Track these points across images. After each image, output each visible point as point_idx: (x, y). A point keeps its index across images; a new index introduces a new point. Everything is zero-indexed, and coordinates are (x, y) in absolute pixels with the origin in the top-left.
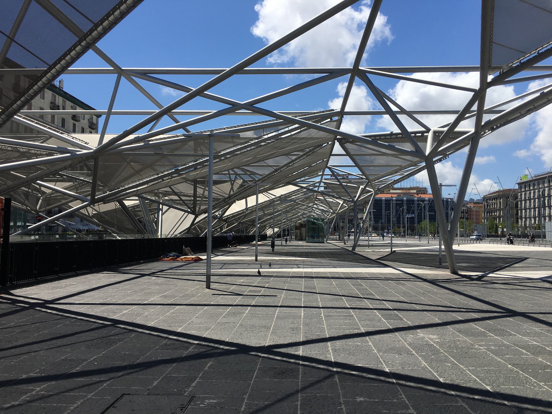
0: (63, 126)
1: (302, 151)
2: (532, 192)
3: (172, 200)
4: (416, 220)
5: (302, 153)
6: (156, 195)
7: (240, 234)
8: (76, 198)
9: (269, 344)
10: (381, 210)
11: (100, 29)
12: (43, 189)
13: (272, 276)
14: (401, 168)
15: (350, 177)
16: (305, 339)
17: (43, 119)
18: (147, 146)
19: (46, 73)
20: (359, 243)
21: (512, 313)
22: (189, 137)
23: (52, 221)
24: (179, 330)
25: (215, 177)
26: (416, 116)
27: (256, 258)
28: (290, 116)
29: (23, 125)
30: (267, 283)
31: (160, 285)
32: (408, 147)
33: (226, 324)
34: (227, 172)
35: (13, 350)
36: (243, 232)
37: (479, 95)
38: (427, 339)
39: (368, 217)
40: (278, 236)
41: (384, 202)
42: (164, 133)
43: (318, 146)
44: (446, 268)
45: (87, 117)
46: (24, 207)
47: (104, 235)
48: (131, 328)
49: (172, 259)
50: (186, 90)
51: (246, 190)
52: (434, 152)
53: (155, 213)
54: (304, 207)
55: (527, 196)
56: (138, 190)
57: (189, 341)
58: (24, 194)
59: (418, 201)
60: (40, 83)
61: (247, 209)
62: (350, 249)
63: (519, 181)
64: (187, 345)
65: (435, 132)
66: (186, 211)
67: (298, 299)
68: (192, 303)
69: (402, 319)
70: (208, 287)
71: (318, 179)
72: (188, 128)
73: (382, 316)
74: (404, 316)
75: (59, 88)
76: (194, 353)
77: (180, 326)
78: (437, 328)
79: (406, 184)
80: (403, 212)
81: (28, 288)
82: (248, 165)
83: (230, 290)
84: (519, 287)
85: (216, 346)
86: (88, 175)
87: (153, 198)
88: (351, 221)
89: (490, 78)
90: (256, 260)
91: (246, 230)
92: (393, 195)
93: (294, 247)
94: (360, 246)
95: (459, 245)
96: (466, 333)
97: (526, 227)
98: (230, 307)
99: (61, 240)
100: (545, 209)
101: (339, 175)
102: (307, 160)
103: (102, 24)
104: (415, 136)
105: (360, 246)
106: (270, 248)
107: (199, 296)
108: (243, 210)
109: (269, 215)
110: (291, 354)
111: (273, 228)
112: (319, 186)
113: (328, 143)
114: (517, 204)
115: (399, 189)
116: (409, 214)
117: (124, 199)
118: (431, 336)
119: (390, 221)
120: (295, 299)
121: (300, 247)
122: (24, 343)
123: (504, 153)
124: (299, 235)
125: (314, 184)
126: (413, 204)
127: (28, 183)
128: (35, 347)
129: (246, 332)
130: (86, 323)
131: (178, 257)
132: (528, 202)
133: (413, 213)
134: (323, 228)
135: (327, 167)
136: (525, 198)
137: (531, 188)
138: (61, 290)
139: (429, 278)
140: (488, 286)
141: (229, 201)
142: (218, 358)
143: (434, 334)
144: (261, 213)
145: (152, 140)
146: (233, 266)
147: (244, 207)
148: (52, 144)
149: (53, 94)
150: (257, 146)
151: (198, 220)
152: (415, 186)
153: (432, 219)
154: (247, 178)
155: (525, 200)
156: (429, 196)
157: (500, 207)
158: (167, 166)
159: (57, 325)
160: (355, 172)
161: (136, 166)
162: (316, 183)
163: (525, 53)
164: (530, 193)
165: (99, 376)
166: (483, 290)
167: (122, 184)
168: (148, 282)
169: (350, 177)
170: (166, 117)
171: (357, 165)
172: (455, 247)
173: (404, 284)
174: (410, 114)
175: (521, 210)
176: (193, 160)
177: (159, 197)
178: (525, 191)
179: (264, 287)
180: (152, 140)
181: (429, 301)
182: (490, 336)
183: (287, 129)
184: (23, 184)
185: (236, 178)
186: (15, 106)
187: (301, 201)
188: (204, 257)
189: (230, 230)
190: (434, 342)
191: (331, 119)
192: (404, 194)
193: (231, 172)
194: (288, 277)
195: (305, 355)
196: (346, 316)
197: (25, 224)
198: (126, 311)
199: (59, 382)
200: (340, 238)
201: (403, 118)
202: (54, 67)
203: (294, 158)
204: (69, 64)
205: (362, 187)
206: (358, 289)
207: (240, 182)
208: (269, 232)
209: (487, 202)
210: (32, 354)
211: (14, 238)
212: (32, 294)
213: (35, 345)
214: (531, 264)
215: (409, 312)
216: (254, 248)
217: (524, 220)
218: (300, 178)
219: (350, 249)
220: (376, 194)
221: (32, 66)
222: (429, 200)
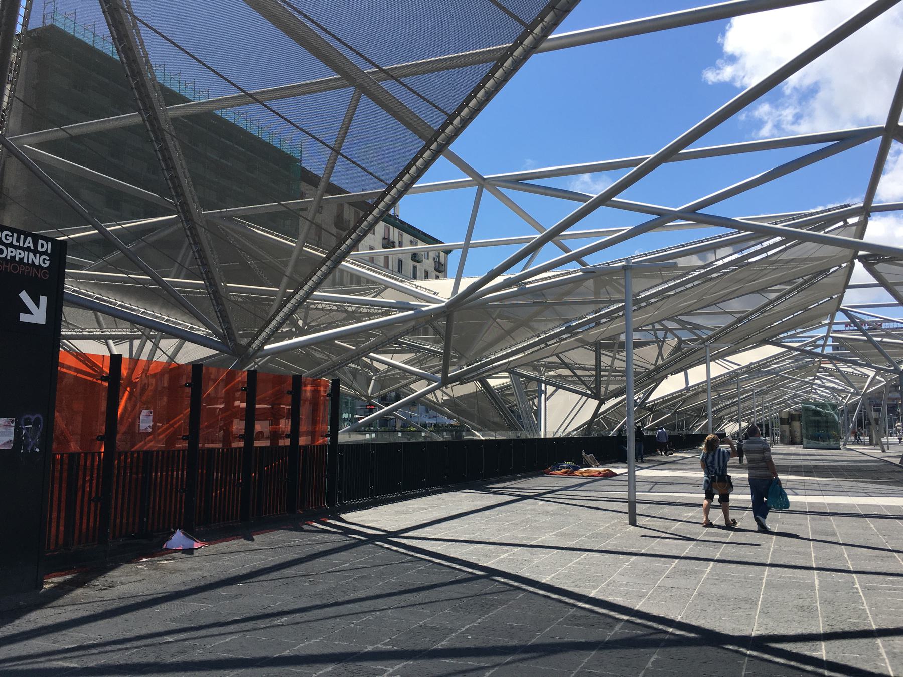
0: (400, 270)
1: (788, 282)
3: (560, 376)
5: (788, 288)
6: (536, 368)
7: (676, 432)
8: (421, 377)
9: (759, 633)
11: (456, 121)
12: (376, 364)
15: (884, 326)
16: (828, 630)
17: (373, 262)
18: (523, 292)
19: (383, 195)
22: (590, 273)
23: (390, 412)
24: (593, 594)
25: (636, 336)
29: (347, 272)
31: (551, 515)
33: (674, 590)
34: (650, 328)
35: (351, 605)
36: (681, 428)
42: (547, 270)
43: (821, 273)
45: (432, 254)
46: (352, 392)
47: (464, 433)
48: (516, 584)
49: (566, 473)
50: (582, 198)
51: (686, 355)
53: (534, 398)
54: (795, 384)
56: (509, 362)
57: (612, 614)
58: (351, 372)
60: (376, 212)
61: (688, 389)
64: (610, 620)
67: (804, 554)
68: (609, 548)
70: (633, 522)
71: (821, 333)
72: (585, 259)
75: (394, 217)
76: (624, 637)
77: (595, 588)
81: (363, 512)
82: (689, 313)
83: (672, 530)
85: (661, 627)
86: (436, 342)
87: (532, 374)
91: (687, 425)
93: (781, 457)
98: (677, 561)
99: (406, 440)
101: (863, 322)
102: (797, 298)
103: (459, 114)
107: (619, 537)
108: (681, 391)
109: (730, 398)
110: (805, 656)
111: (737, 421)
112: (824, 346)
113: (840, 266)
117: (489, 376)
120: (799, 553)
121: (792, 457)
122: (364, 596)
124: (787, 434)
125: (815, 341)
127: (356, 357)
128: (380, 603)
129: (712, 608)
130: (448, 570)
131: (576, 469)
134: (835, 424)
135: (838, 309)
138: (408, 516)
141: (656, 375)
142: (668, 649)
144: (714, 396)
145: (530, 283)
146: (672, 488)
147: (683, 386)
148: (388, 297)
149: (386, 226)
151: (604, 408)
154: (686, 335)
159: (408, 569)
161: (506, 325)
165: (477, 659)
167: (486, 353)
168: (534, 510)
176: (595, 309)
177: (540, 371)
180: (530, 283)
184: (352, 357)
185: (665, 337)
186: (343, 247)
188: (620, 470)
189: (659, 425)
191: (846, 222)
193: (657, 327)
195: (832, 659)
197: (353, 415)
198: (505, 555)
199: (420, 662)
202: (395, 186)
203: (773, 296)
204: (414, 179)
207: (673, 342)
210: (378, 613)
211: (343, 437)
212: (369, 521)
213: (380, 600)
218: (786, 332)
221: (355, 185)
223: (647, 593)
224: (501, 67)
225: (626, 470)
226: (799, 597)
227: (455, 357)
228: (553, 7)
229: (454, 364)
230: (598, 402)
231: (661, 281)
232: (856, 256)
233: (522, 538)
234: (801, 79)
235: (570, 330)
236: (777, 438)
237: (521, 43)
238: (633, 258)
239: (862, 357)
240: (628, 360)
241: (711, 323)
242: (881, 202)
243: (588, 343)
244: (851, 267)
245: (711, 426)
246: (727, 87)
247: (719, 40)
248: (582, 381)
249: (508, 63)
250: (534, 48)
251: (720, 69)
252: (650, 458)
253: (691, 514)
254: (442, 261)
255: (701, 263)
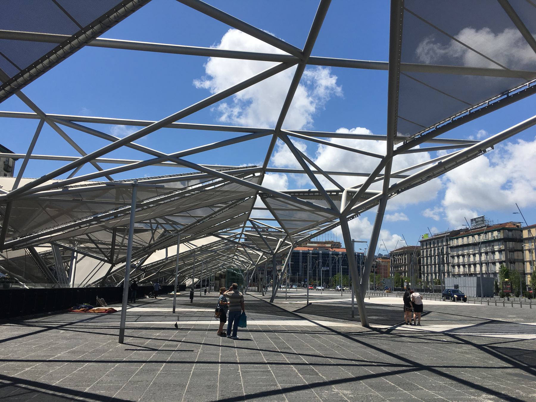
2: (433, 249)
3: (88, 248)
4: (331, 273)
5: (224, 206)
6: (71, 242)
10: (299, 262)
11: (26, 75)
13: (189, 329)
14: (318, 224)
15: (269, 230)
18: (66, 192)
20: (278, 294)
21: (419, 367)
24: (87, 390)
25: (137, 225)
26: (332, 176)
27: (174, 310)
28: (214, 170)
30: (184, 336)
31: (67, 339)
32: (323, 204)
33: (139, 383)
34: (148, 221)
36: (161, 282)
37: (386, 161)
38: (341, 394)
39: (287, 269)
40: (197, 286)
41: (301, 255)
42: (85, 180)
44: (358, 320)
45: (3, 159)
48: (33, 388)
51: (168, 239)
52: (348, 210)
53: (69, 261)
54: (224, 258)
55: (429, 253)
59: (333, 254)
61: (167, 259)
62: (269, 301)
63: (421, 239)
65: (348, 192)
66: (102, 260)
67: (216, 354)
68: (103, 359)
69: (317, 374)
70: (121, 341)
71: (239, 231)
73: (298, 371)
74: (319, 371)
77: (88, 386)
78: (351, 383)
79: (321, 238)
80: (318, 265)
82: (171, 215)
84: (423, 340)
88: (269, 273)
89: (395, 147)
90: (174, 312)
91: (165, 280)
92: (310, 249)
93: (213, 298)
94: (278, 297)
95: (369, 297)
96: (378, 388)
97: (428, 282)
100: (444, 266)
101: (261, 228)
102: (228, 212)
104: (331, 195)
105: (278, 297)
106: (188, 299)
107: (112, 351)
108: (162, 260)
111: (193, 278)
112: (240, 238)
113: (250, 197)
114: (420, 260)
115: (315, 243)
116: (324, 267)
117: (37, 246)
118: (346, 392)
119: (306, 273)
120: (213, 354)
123: (413, 211)
125: (236, 235)
126: (328, 257)
129: (160, 392)
132: (429, 258)
133: (328, 266)
134: (242, 279)
135: (248, 220)
136: (427, 255)
137: (432, 246)
139: (342, 331)
140: (396, 339)
141: (149, 250)
143: (347, 390)
144: (181, 263)
145: (72, 187)
146: (149, 318)
147: (164, 257)
150: (181, 196)
151: (114, 269)
152: (330, 240)
153: (346, 272)
154: (169, 228)
155: (427, 257)
156: (342, 250)
157: (405, 263)
158: (85, 212)
160: (275, 225)
161: (52, 212)
162: (237, 235)
163: (424, 127)
164: (431, 250)
166: (392, 343)
168: (56, 336)
169: (269, 230)
170: (88, 164)
171: (277, 219)
172: (366, 300)
173: (320, 338)
174: (326, 174)
175: (424, 266)
177: (74, 244)
178: (427, 248)
179: (181, 341)
180: (72, 187)
181: (343, 354)
182: (399, 390)
183: (211, 182)
187: (222, 252)
190: (348, 398)
192: (319, 247)
193: (153, 221)
194: (206, 330)
196: (263, 371)
198: (29, 369)
200: (258, 289)
201: (320, 178)
205: (281, 240)
206: (276, 343)
207: (161, 231)
208: (188, 282)
209: (394, 258)
214: (434, 318)
215: (324, 367)
216: (173, 299)
217: (426, 275)
218: (222, 230)
219: (269, 301)
220: (294, 247)
222: (342, 254)
223: (122, 386)
224: (60, 50)
225: (120, 309)
226: (209, 380)
227: (11, 231)
228: (100, 22)
229: (9, 236)
230: (110, 265)
231: (156, 195)
232: (257, 193)
233: (44, 356)
234: (243, 96)
235: (96, 219)
236: (213, 288)
237: (77, 38)
238: (141, 179)
239: (257, 245)
240: (129, 240)
241: (182, 221)
242: (276, 167)
243: (108, 228)
244: (255, 198)
245: (177, 281)
246: (206, 91)
247: (204, 65)
248: (102, 251)
249: (67, 47)
250: (86, 42)
251: (203, 81)
252: (140, 300)
253: (158, 334)
254: (11, 164)
255: (182, 187)
